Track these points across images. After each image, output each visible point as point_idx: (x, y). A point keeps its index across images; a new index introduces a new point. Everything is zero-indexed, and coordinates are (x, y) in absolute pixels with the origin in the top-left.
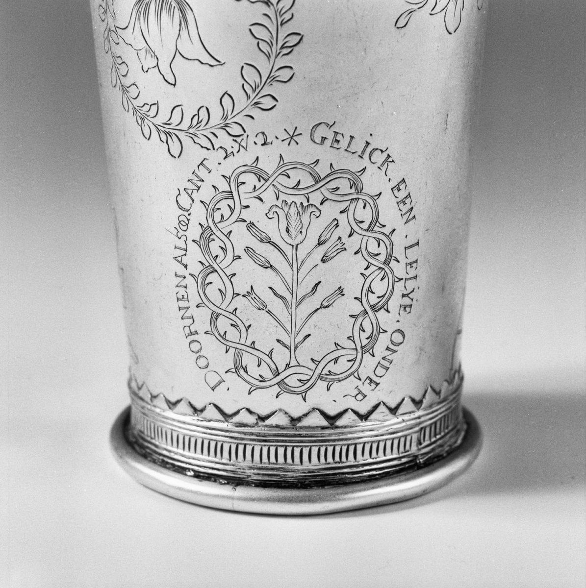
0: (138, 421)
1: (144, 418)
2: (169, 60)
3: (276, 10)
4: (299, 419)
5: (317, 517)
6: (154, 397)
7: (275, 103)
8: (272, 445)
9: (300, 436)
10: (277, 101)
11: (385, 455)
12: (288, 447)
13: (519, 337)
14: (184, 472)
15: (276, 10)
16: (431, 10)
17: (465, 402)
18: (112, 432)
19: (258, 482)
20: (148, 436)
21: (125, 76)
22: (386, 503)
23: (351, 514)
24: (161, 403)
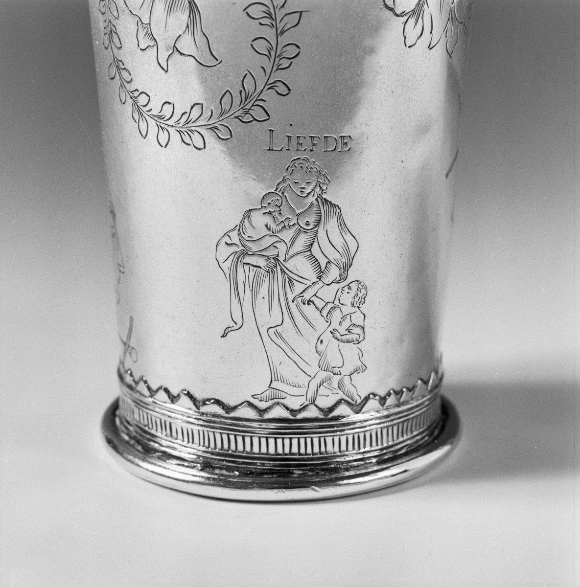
0: (131, 413)
1: (147, 413)
2: (160, 71)
3: (124, 88)
4: (331, 409)
5: (312, 503)
6: (153, 392)
7: (164, 146)
8: (302, 437)
9: (214, 422)
10: (165, 147)
11: (377, 445)
12: (253, 438)
13: (506, 326)
14: (205, 460)
15: (275, 6)
16: (301, 53)
17: (443, 391)
18: (103, 423)
19: (131, 457)
20: (145, 426)
21: (129, 82)
22: (373, 490)
23: (345, 499)
24: (162, 396)
